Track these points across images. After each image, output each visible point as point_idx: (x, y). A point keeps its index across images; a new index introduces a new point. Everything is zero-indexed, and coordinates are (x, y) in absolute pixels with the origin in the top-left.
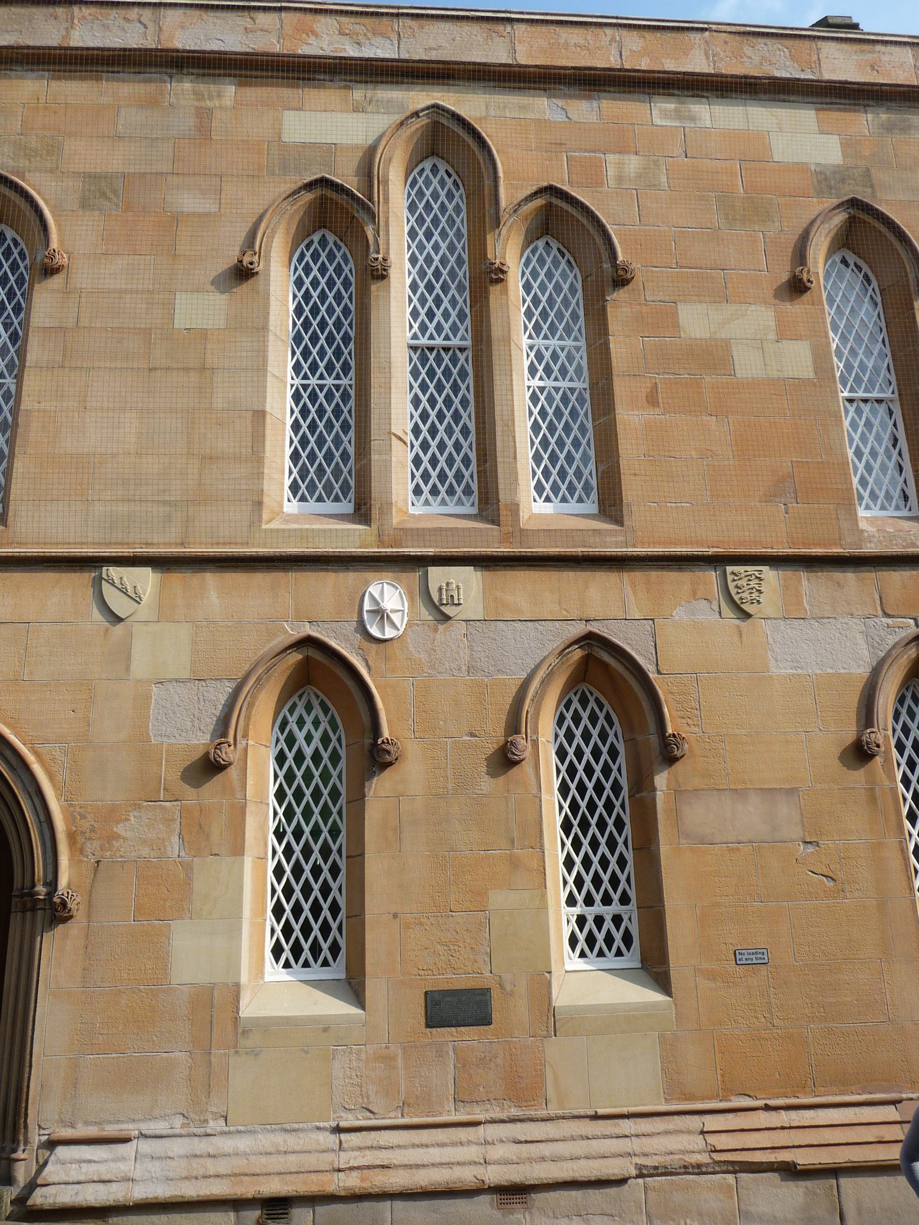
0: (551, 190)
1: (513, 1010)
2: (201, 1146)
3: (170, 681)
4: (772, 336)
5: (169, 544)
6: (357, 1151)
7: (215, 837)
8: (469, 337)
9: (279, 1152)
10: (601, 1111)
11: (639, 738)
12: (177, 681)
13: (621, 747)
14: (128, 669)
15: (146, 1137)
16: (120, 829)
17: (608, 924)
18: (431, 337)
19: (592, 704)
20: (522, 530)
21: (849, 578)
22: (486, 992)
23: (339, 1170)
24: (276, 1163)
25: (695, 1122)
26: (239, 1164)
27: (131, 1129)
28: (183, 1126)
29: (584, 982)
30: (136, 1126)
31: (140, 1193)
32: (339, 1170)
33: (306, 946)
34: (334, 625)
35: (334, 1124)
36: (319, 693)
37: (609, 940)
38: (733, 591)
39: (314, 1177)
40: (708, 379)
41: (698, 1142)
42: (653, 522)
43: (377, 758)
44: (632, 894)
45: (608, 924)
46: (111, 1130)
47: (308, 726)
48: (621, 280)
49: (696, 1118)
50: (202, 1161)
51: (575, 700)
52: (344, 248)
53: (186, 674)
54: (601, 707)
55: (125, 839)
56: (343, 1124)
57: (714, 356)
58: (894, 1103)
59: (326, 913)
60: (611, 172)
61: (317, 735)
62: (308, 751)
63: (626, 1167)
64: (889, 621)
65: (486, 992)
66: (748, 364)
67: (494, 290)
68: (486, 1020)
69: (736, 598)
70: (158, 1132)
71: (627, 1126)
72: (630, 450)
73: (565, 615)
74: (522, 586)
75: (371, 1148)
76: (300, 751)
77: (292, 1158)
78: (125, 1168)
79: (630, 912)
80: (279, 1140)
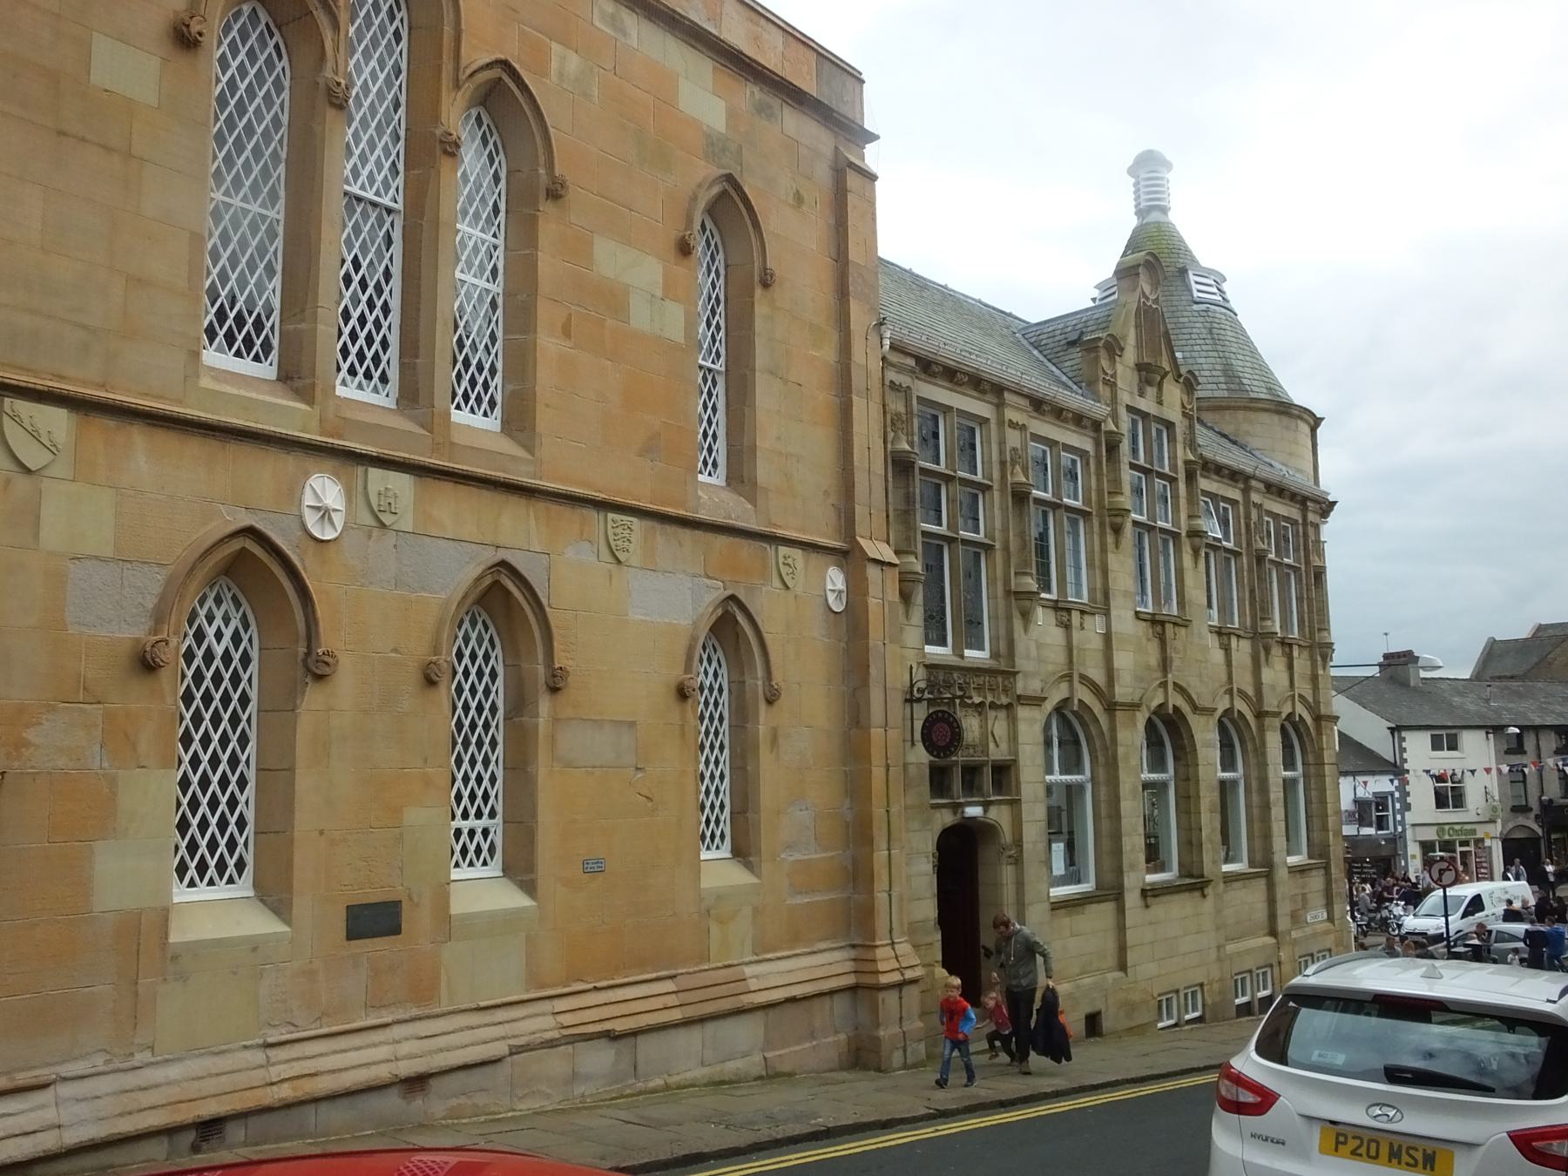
0: (505, 65)
1: (417, 921)
2: (130, 1080)
3: (90, 557)
4: (659, 293)
5: (85, 383)
6: (285, 1064)
7: (143, 747)
8: (400, 199)
9: (211, 1075)
10: (483, 1004)
11: (524, 665)
12: (97, 558)
13: (500, 670)
14: (36, 536)
15: (65, 1079)
16: (30, 735)
17: (478, 837)
18: (377, 194)
19: (480, 626)
20: (452, 444)
21: (686, 534)
22: (397, 904)
23: (272, 1084)
24: (210, 1086)
25: (546, 1006)
26: (173, 1093)
27: (45, 1074)
28: (107, 1062)
29: (480, 889)
30: (53, 1069)
31: (72, 1137)
32: (272, 1084)
33: (212, 863)
34: (271, 515)
35: (261, 1041)
36: (232, 585)
37: (478, 851)
38: (611, 537)
39: (248, 1093)
40: (609, 322)
41: (549, 1022)
42: (562, 461)
43: (317, 670)
44: (499, 809)
45: (478, 837)
46: (22, 1078)
47: (218, 621)
48: (555, 193)
49: (547, 1002)
50: (132, 1095)
51: (467, 619)
52: (277, 37)
53: (108, 552)
54: (487, 629)
55: (37, 747)
56: (270, 1040)
57: (613, 299)
58: (672, 977)
59: (232, 828)
60: (554, 65)
61: (228, 633)
62: (219, 650)
63: (500, 1049)
64: (708, 581)
65: (397, 904)
66: (641, 317)
67: (445, 164)
68: (397, 930)
69: (613, 544)
70: (80, 1073)
71: (501, 1015)
72: (545, 378)
73: (480, 539)
74: (451, 506)
75: (298, 1059)
76: (209, 649)
77: (223, 1079)
78: (50, 1115)
79: (496, 826)
80: (210, 1064)
